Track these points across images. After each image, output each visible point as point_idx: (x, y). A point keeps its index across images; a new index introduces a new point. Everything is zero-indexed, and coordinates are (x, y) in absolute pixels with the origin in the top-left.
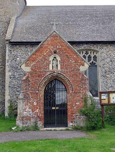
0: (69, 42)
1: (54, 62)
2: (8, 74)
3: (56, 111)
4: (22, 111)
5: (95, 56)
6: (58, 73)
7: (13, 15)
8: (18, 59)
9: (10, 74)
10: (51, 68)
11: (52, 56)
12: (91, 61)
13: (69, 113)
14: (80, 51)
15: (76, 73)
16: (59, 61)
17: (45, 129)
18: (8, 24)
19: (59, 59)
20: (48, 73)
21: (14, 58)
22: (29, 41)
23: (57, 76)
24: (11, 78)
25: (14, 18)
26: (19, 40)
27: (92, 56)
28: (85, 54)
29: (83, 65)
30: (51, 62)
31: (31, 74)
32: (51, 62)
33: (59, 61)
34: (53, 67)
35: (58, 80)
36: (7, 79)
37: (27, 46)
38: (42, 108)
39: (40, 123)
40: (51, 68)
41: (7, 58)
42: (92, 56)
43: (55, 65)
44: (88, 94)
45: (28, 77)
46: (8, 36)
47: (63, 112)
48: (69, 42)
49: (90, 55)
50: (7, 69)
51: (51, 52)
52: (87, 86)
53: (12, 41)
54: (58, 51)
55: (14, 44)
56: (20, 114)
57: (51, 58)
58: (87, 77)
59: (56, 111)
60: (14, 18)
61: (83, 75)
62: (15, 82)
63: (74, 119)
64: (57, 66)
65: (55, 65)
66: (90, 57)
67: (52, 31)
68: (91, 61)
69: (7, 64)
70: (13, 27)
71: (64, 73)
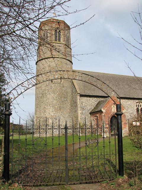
9: (81, 112)
20: (112, 113)
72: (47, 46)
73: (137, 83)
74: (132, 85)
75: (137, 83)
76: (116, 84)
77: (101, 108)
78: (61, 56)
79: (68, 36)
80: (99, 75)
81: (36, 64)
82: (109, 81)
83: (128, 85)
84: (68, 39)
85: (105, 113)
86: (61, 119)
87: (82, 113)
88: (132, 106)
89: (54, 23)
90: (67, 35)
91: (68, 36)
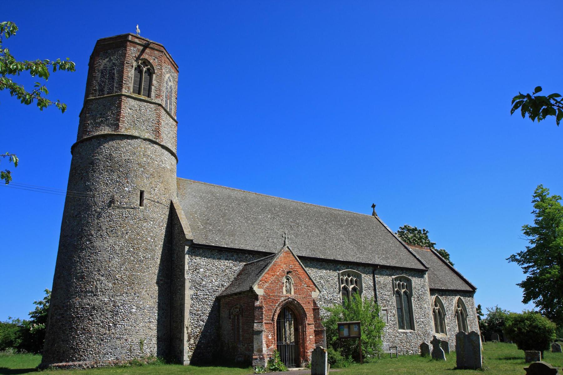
0: (298, 256)
8: (202, 270)
9: (192, 292)
10: (285, 292)
20: (283, 299)
21: (196, 269)
24: (192, 299)
48: (298, 256)
72: (353, 305)
73: (342, 226)
74: (330, 228)
75: (342, 226)
76: (290, 224)
77: (253, 283)
78: (147, 136)
79: (171, 87)
80: (245, 197)
81: (72, 153)
82: (272, 213)
83: (320, 227)
84: (171, 96)
85: (264, 298)
86: (131, 313)
87: (195, 297)
88: (332, 281)
89: (135, 47)
90: (170, 84)
91: (171, 87)
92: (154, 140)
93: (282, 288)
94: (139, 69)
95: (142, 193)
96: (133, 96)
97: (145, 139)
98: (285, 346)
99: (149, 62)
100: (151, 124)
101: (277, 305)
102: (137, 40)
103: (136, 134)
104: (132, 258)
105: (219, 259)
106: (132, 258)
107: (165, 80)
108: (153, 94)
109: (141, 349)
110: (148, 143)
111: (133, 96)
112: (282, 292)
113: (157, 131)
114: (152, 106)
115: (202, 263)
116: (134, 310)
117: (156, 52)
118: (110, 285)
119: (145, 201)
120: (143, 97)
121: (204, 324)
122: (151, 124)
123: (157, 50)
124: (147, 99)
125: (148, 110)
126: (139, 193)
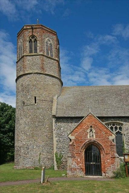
0: (98, 117)
1: (91, 133)
2: (55, 139)
3: (93, 165)
4: (70, 164)
5: (120, 127)
6: (94, 141)
7: (55, 95)
8: (62, 128)
9: (57, 139)
10: (89, 137)
11: (89, 129)
12: (117, 131)
13: (102, 167)
14: (108, 124)
15: (106, 140)
16: (95, 133)
17: (86, 176)
18: (52, 102)
19: (94, 131)
20: (87, 141)
21: (59, 128)
22: (70, 116)
23: (93, 142)
24: (57, 142)
25: (55, 98)
26: (62, 116)
27: (118, 127)
28: (113, 128)
29: (111, 136)
30: (89, 133)
31: (75, 141)
32: (89, 133)
33: (95, 133)
34: (90, 136)
35: (94, 145)
36: (55, 143)
37: (68, 120)
38: (84, 163)
39: (83, 173)
40: (89, 137)
41: (54, 128)
42: (118, 127)
43: (91, 136)
44: (116, 155)
45: (73, 143)
46: (54, 113)
47: (41, 175)
48: (98, 117)
49: (116, 126)
50: (54, 136)
51: (88, 126)
52: (115, 150)
53: (57, 116)
54: (93, 126)
55: (59, 119)
56: (70, 166)
57: (88, 131)
58: (114, 143)
59: (93, 165)
60: (55, 98)
61: (111, 142)
62: (60, 145)
63: (106, 171)
64: (93, 136)
65: (91, 135)
66: (116, 128)
67: (89, 113)
68: (115, 126)
69: (54, 132)
70: (56, 105)
71: (98, 141)
89: (27, 31)
92: (41, 72)
93: (87, 135)
94: (30, 41)
95: (35, 98)
96: (31, 55)
97: (35, 73)
98: (92, 164)
99: (35, 36)
100: (38, 65)
101: (83, 144)
102: (28, 27)
103: (31, 72)
104: (33, 126)
105: (72, 123)
106: (33, 126)
107: (45, 41)
108: (38, 51)
109: (39, 163)
110: (37, 74)
111: (29, 54)
112: (87, 137)
113: (43, 68)
114: (38, 56)
115: (62, 125)
116: (35, 147)
117: (38, 29)
118: (25, 137)
119: (37, 101)
120: (34, 54)
121: (128, 151)
122: (38, 65)
123: (38, 28)
124: (36, 54)
125: (38, 59)
126: (34, 98)
